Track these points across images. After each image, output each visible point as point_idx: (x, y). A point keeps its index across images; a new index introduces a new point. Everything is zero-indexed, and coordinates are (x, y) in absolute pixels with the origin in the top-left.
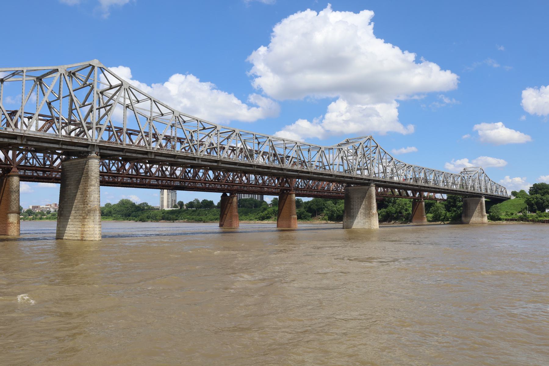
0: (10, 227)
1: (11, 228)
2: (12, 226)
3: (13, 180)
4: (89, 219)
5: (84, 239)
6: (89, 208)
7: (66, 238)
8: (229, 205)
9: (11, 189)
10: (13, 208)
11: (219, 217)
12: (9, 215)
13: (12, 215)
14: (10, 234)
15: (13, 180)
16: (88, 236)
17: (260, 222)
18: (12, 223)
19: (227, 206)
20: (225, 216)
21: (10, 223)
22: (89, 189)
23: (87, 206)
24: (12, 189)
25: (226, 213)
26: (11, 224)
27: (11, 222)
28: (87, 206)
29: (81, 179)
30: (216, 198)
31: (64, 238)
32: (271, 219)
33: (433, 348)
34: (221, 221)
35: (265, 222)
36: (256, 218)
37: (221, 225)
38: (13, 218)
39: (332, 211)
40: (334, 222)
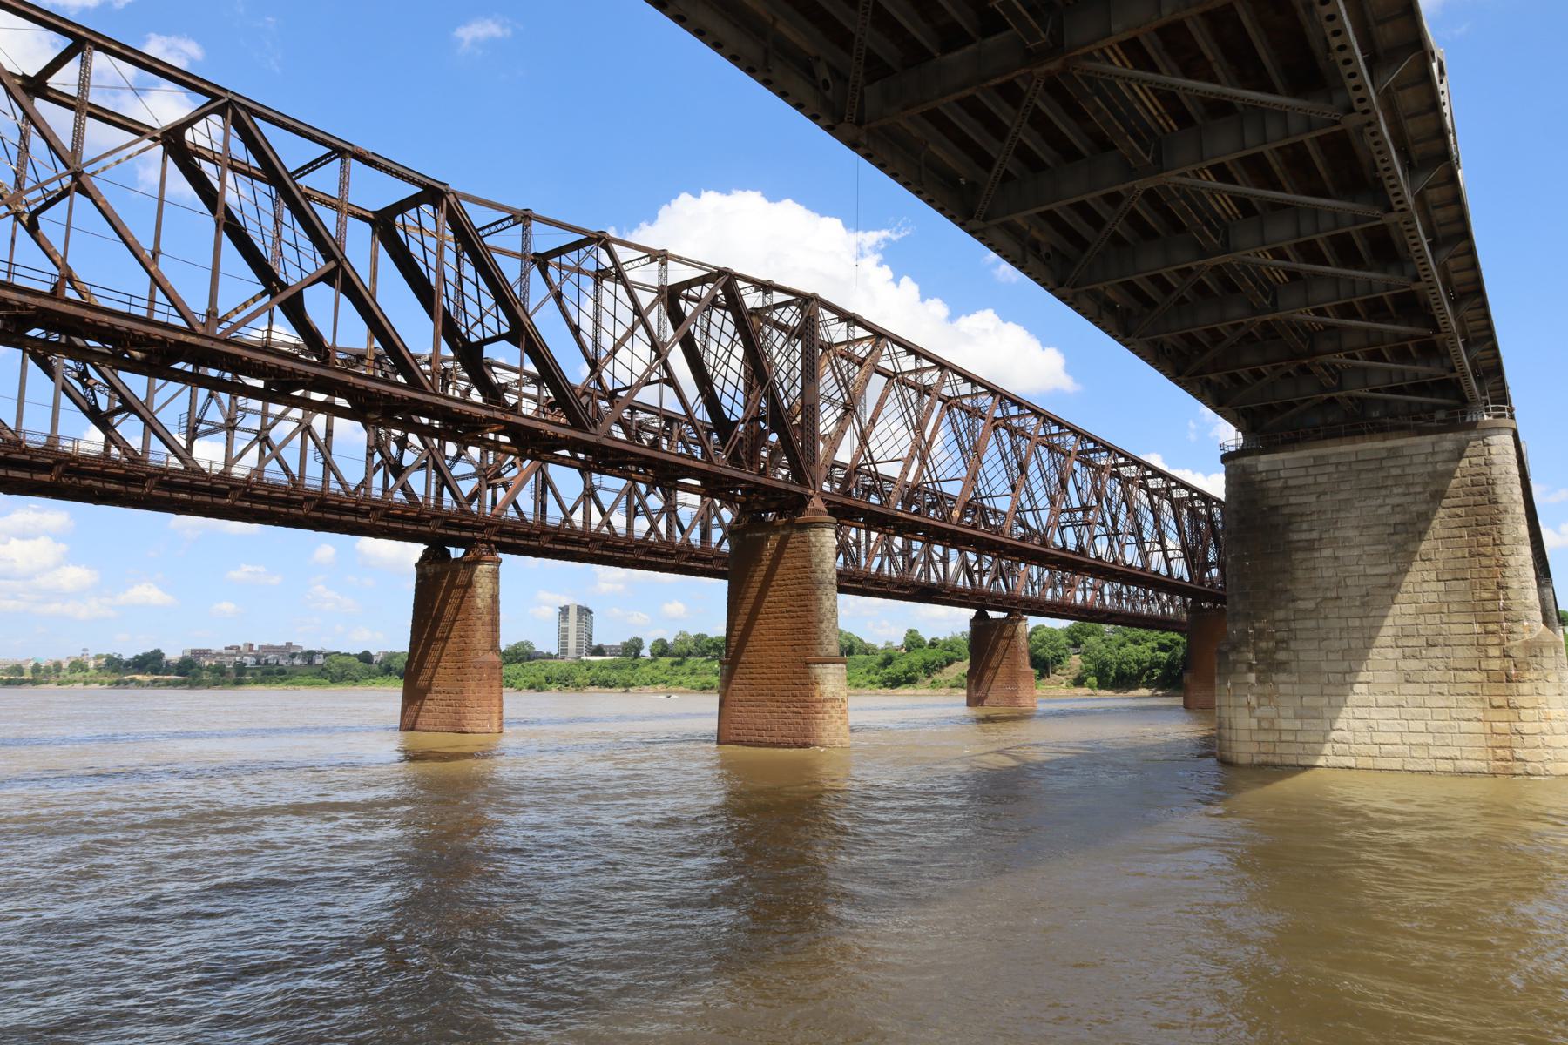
0: (827, 717)
1: (831, 717)
2: (833, 712)
3: (824, 540)
4: (1539, 684)
5: (1518, 767)
6: (1527, 636)
7: (1333, 761)
8: (1003, 643)
9: (819, 575)
10: (830, 643)
11: (715, 680)
12: (819, 670)
13: (829, 671)
14: (827, 741)
15: (824, 540)
16: (1547, 754)
17: (889, 691)
18: (835, 700)
19: (994, 648)
20: (989, 674)
21: (826, 700)
22: (1512, 554)
23: (1516, 628)
24: (823, 572)
25: (993, 664)
26: (828, 705)
27: (828, 695)
28: (1516, 628)
29: (1426, 518)
30: (953, 622)
31: (1321, 761)
32: (918, 685)
33: (168, 887)
34: (414, 695)
35: (901, 690)
36: (872, 682)
37: (972, 702)
38: (831, 680)
39: (1105, 664)
40: (1110, 693)
